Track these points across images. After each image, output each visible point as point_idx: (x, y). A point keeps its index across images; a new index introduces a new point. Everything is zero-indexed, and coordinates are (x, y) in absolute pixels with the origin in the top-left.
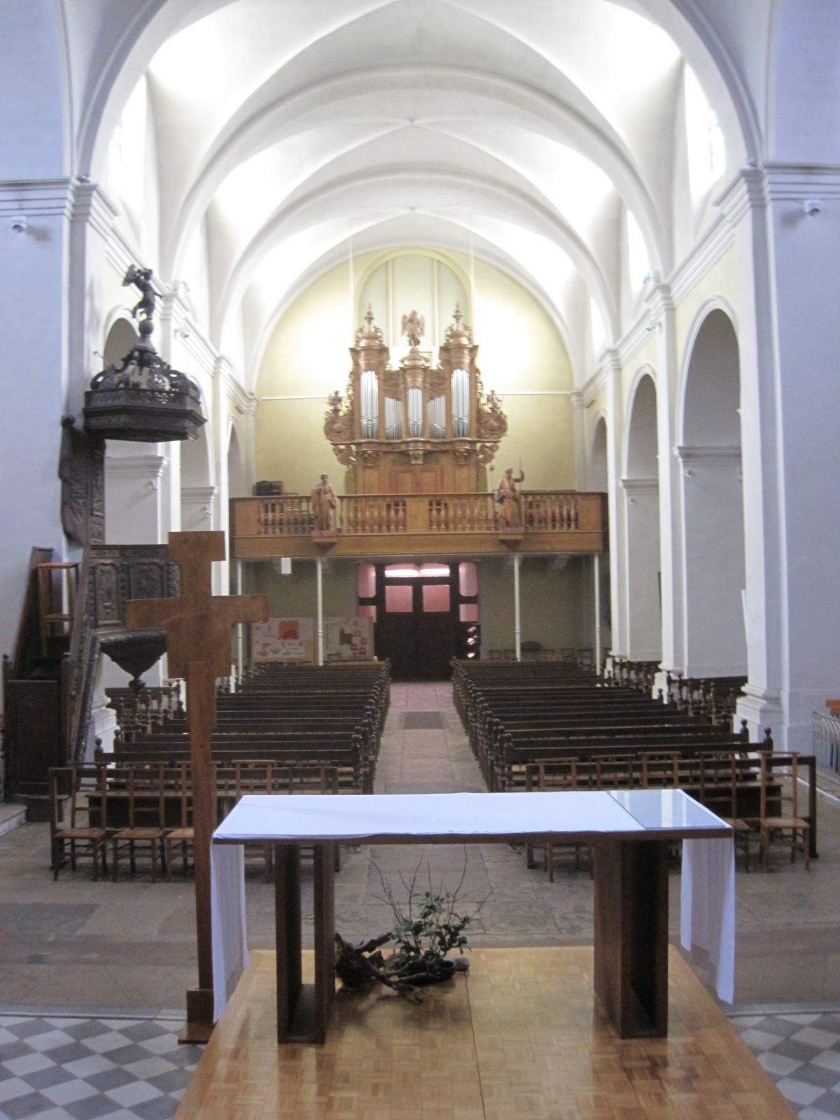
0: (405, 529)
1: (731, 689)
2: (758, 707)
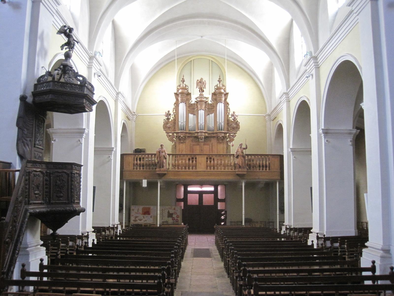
0: (196, 169)
1: (346, 241)
2: (379, 255)
